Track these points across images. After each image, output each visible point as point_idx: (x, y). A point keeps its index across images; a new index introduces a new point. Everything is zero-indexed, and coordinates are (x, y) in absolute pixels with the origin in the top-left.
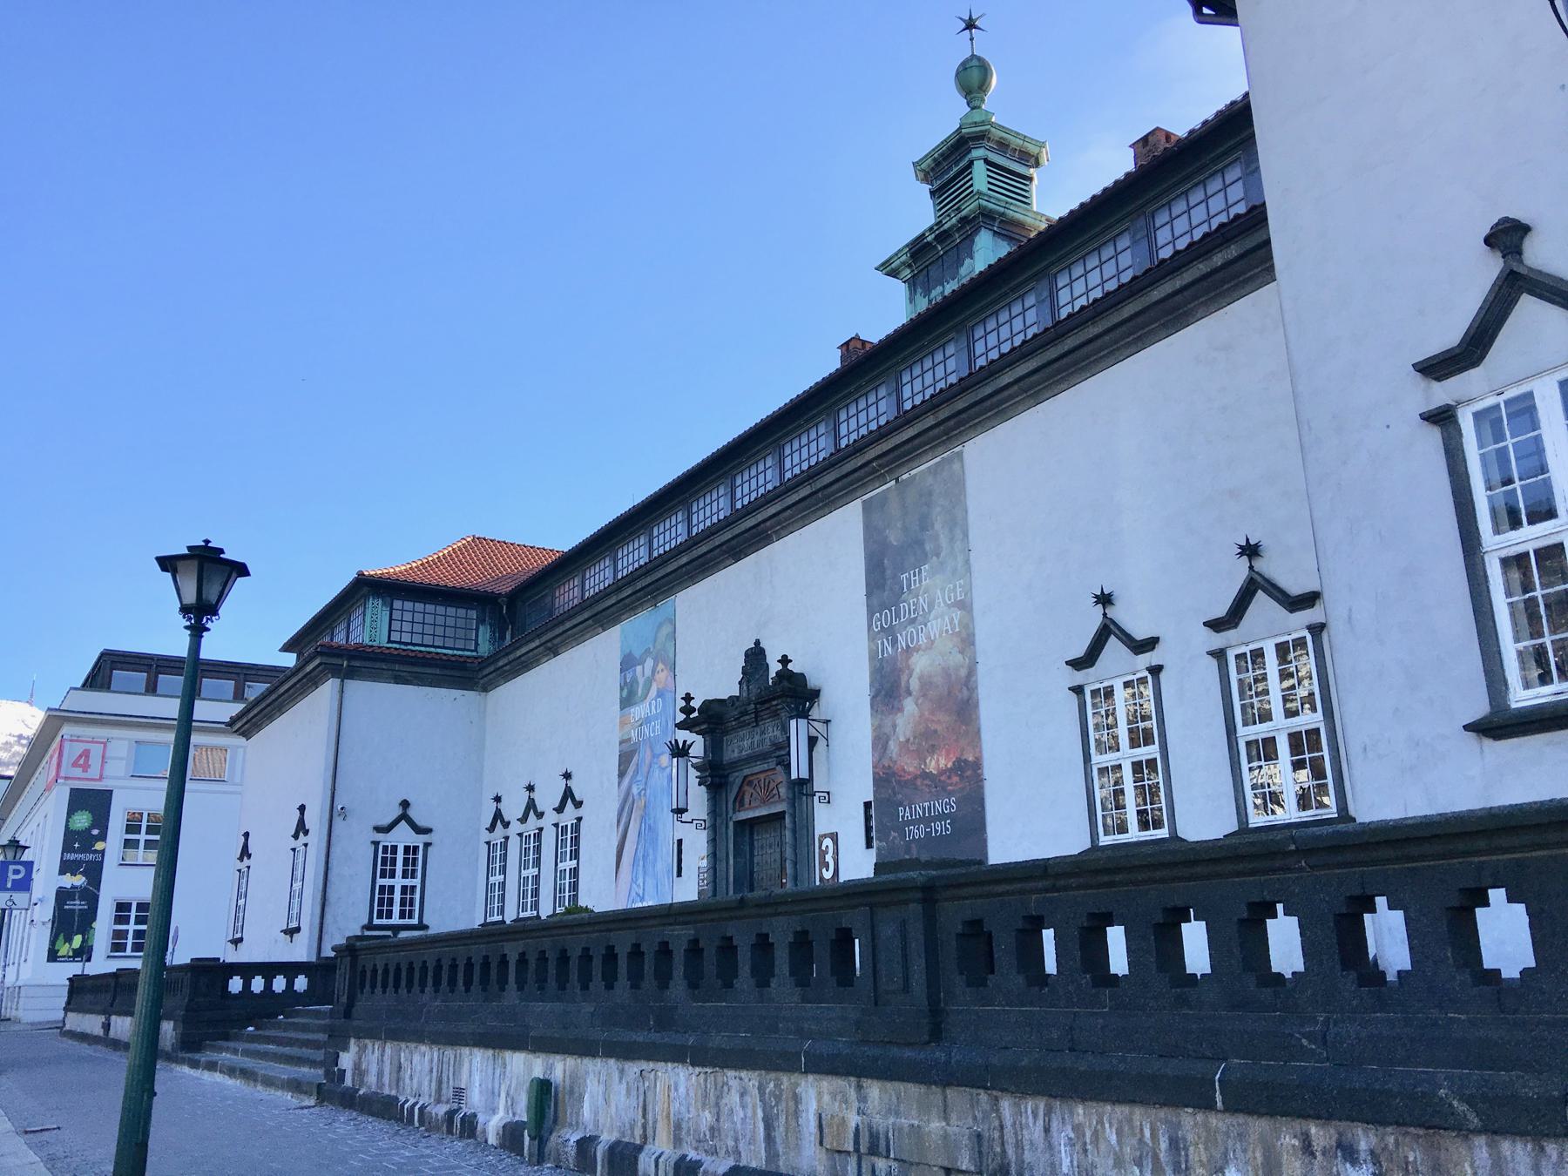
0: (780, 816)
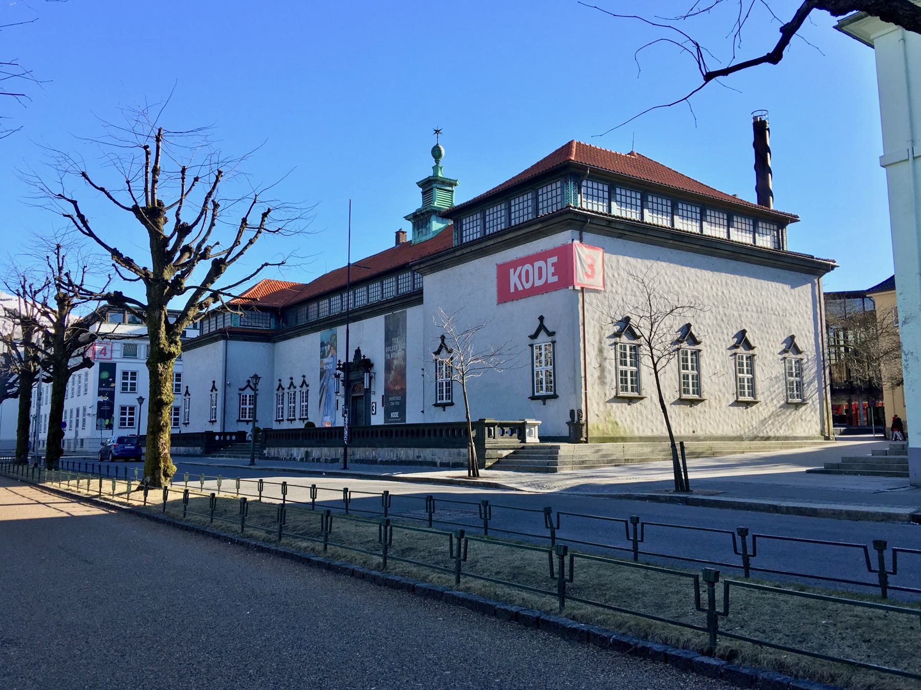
0: (362, 396)
